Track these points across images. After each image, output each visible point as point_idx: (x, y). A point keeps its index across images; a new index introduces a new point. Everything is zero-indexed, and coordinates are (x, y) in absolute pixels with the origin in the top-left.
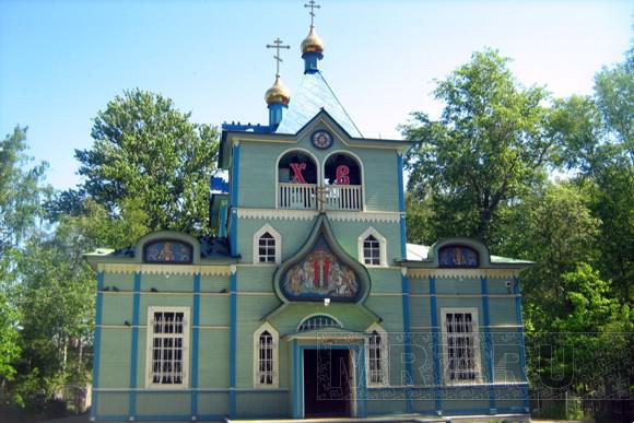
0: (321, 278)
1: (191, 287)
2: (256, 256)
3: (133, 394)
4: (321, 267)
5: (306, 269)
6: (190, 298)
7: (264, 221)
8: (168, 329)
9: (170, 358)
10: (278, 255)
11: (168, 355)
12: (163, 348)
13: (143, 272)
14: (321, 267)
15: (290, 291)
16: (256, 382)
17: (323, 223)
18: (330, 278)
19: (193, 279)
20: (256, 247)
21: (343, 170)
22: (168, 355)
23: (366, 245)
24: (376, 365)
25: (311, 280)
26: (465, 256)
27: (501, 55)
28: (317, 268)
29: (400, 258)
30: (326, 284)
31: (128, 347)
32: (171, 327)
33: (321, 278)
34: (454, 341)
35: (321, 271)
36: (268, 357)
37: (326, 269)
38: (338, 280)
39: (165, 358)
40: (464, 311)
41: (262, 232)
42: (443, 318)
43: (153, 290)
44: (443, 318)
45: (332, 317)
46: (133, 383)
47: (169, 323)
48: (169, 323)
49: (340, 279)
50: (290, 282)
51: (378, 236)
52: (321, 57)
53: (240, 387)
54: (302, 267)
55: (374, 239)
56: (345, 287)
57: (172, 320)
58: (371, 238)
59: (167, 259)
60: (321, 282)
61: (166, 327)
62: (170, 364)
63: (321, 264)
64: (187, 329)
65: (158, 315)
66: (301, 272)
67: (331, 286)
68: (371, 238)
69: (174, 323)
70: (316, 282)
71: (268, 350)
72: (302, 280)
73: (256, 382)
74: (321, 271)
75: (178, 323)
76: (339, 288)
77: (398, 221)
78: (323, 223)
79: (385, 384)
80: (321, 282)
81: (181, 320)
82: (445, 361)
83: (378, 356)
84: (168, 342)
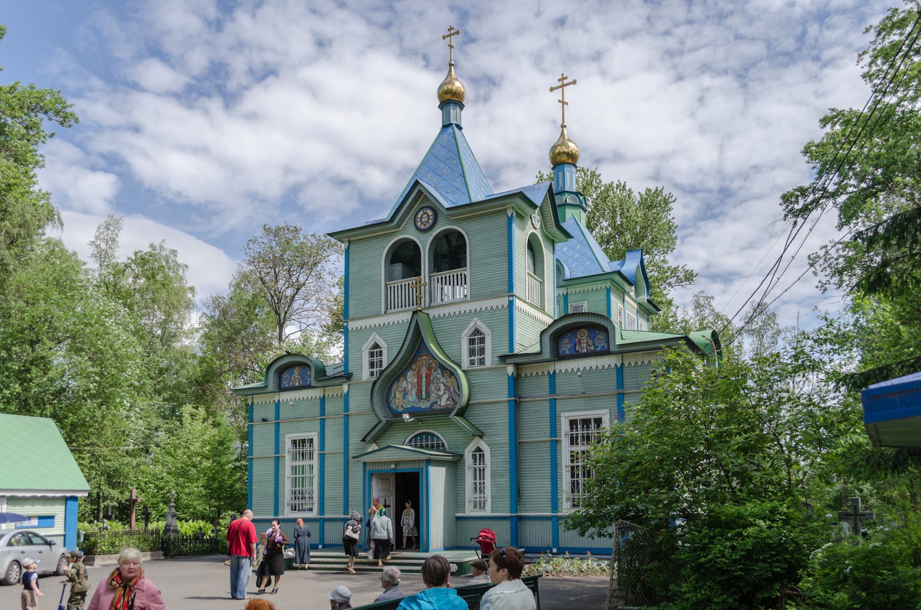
0: (424, 388)
1: (317, 410)
4: (424, 375)
5: (409, 380)
6: (317, 424)
14: (424, 375)
15: (394, 406)
16: (612, 540)
17: (417, 322)
18: (432, 387)
19: (614, 373)
24: (479, 488)
25: (414, 392)
26: (593, 339)
27: (180, 259)
28: (419, 377)
29: (505, 351)
31: (272, 477)
33: (424, 388)
34: (308, 456)
35: (424, 380)
36: (475, 484)
37: (428, 376)
38: (439, 390)
40: (591, 414)
41: (368, 344)
42: (565, 427)
43: (264, 420)
45: (436, 433)
49: (442, 387)
51: (484, 329)
54: (406, 379)
56: (446, 396)
59: (297, 384)
60: (424, 393)
63: (424, 371)
67: (433, 397)
71: (475, 479)
72: (405, 393)
73: (612, 540)
74: (424, 380)
76: (440, 397)
78: (417, 322)
79: (488, 512)
80: (424, 393)
83: (475, 484)
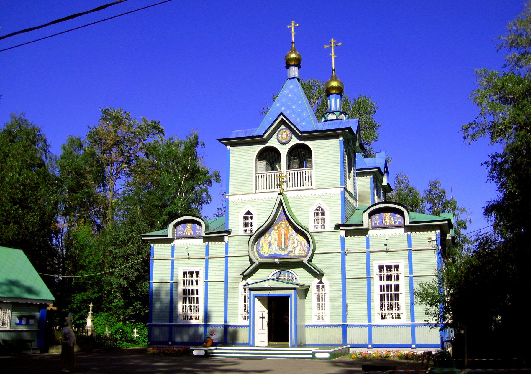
3: (171, 327)
8: (389, 278)
9: (392, 300)
18: (289, 242)
22: (390, 297)
25: (276, 244)
28: (280, 235)
30: (286, 247)
32: (391, 276)
39: (388, 300)
49: (296, 242)
52: (286, 67)
55: (251, 214)
56: (299, 248)
57: (391, 270)
61: (387, 276)
62: (391, 305)
65: (381, 268)
66: (269, 239)
67: (289, 249)
69: (392, 273)
80: (283, 245)
81: (397, 270)
82: (376, 302)
84: (389, 288)
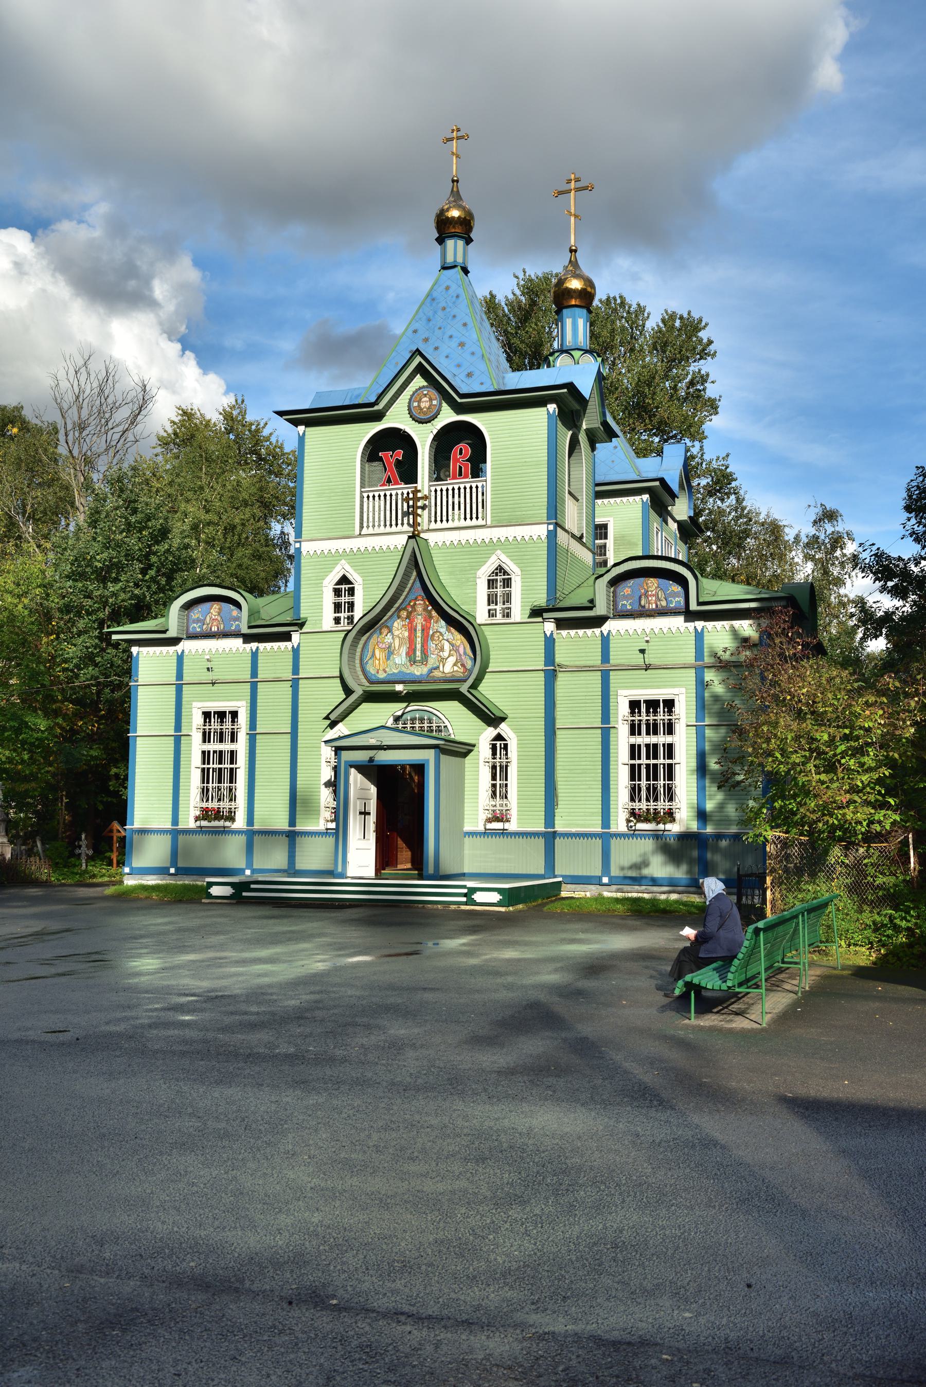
0: (419, 646)
2: (329, 613)
4: (419, 627)
5: (396, 633)
7: (492, 546)
10: (358, 613)
11: (653, 772)
12: (643, 761)
13: (614, 632)
14: (419, 627)
18: (432, 645)
20: (329, 599)
21: (462, 451)
22: (653, 772)
23: (491, 583)
25: (404, 650)
28: (412, 630)
32: (655, 725)
33: (419, 646)
37: (425, 629)
38: (442, 650)
39: (648, 779)
44: (623, 709)
46: (175, 821)
47: (651, 718)
48: (651, 718)
49: (447, 646)
50: (373, 654)
53: (181, 826)
57: (655, 712)
58: (500, 570)
59: (214, 629)
60: (418, 653)
62: (655, 789)
64: (242, 737)
67: (432, 660)
68: (500, 570)
70: (411, 652)
72: (390, 652)
74: (419, 634)
75: (637, 718)
76: (443, 660)
77: (544, 537)
80: (418, 653)
81: (670, 712)
84: (653, 750)
